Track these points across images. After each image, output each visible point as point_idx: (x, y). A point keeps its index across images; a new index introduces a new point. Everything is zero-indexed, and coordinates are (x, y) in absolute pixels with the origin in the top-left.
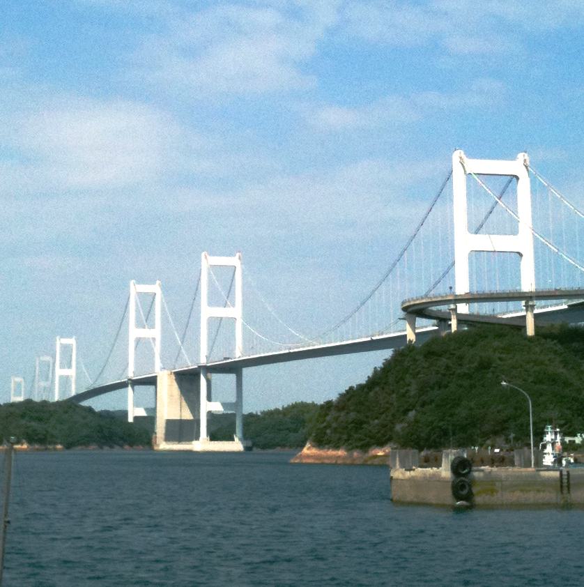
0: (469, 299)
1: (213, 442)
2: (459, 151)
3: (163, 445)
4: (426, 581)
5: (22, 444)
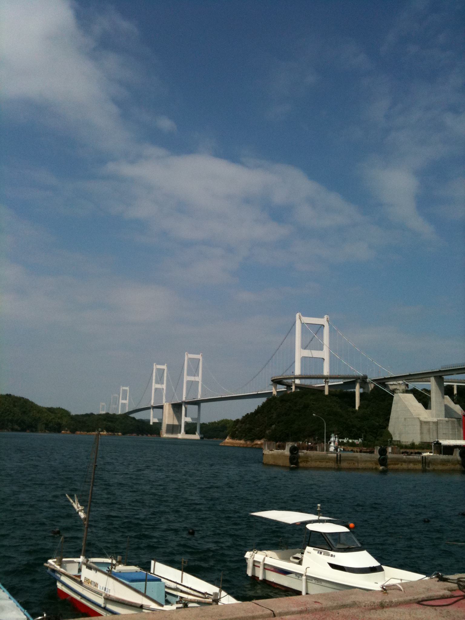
5: (104, 432)
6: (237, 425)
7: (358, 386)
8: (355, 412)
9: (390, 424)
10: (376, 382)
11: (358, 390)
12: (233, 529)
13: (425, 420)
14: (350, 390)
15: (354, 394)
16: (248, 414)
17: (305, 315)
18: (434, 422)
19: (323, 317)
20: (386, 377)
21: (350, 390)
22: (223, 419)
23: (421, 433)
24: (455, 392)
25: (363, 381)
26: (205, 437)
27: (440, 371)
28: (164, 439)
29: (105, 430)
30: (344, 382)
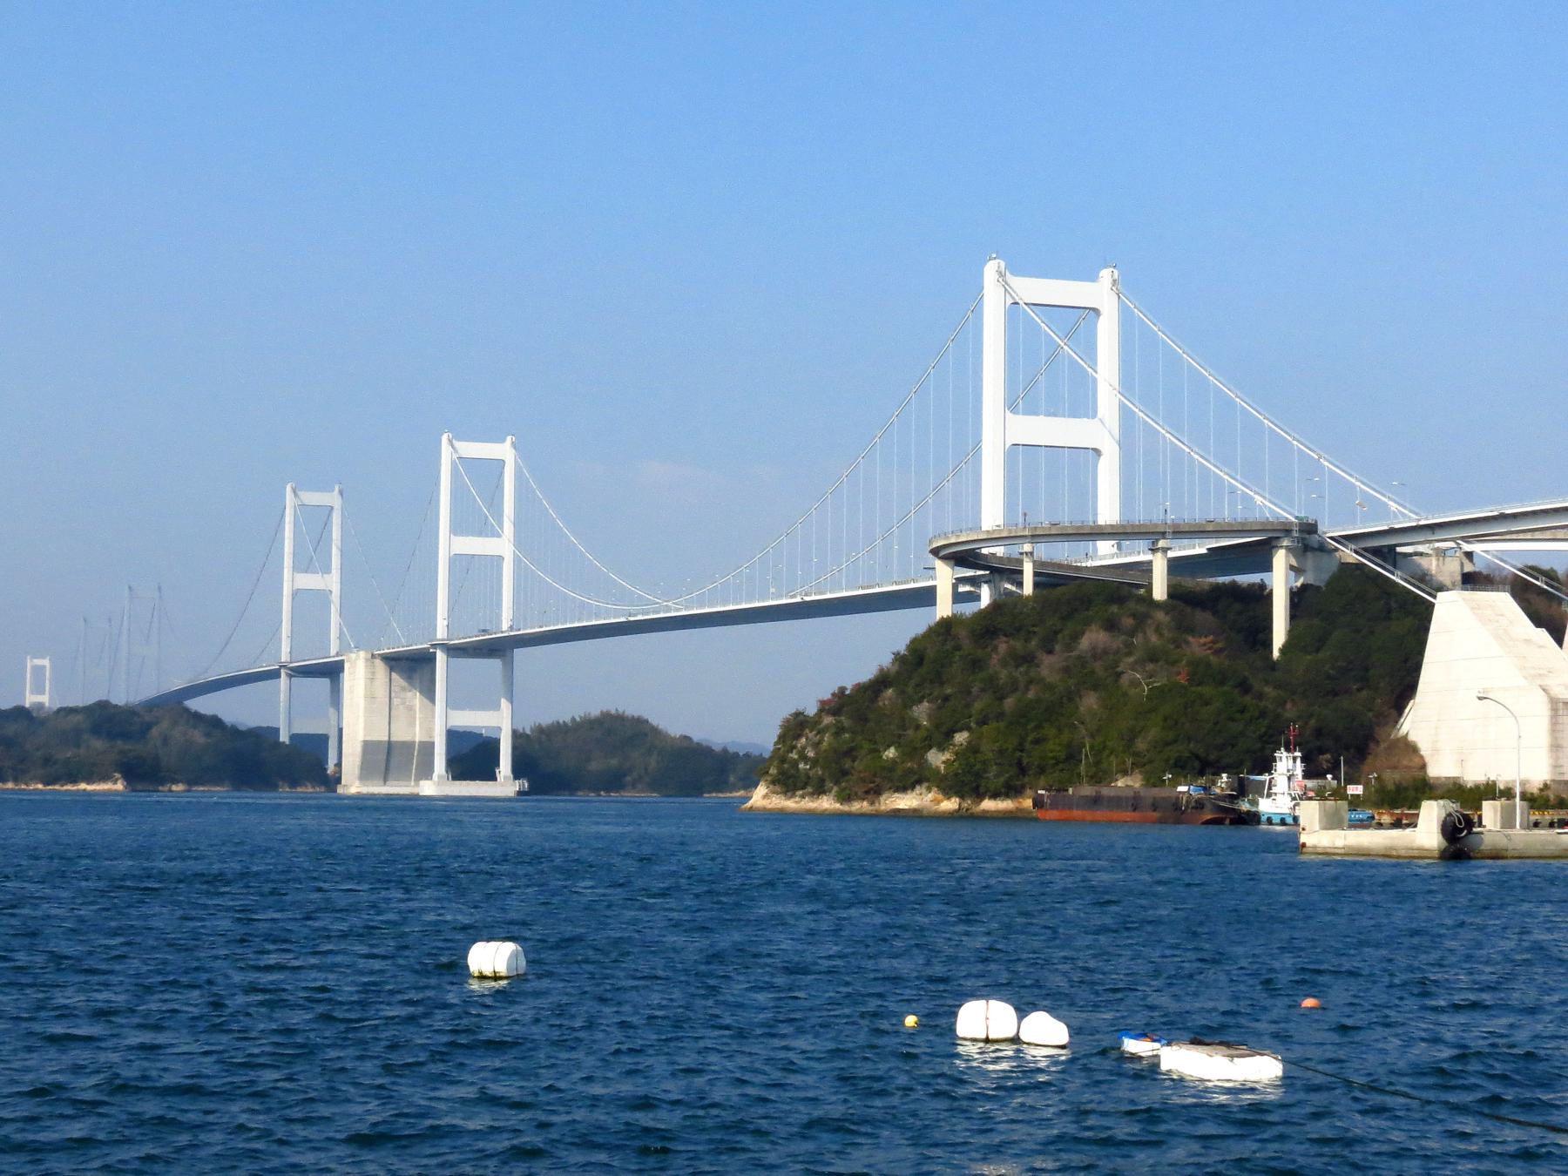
0: (1118, 533)
1: (458, 782)
2: (997, 261)
3: (353, 785)
4: (1252, 999)
5: (115, 783)
6: (798, 737)
7: (1280, 559)
8: (1273, 666)
10: (1353, 547)
11: (1280, 579)
14: (1212, 580)
15: (1262, 597)
16: (842, 690)
17: (1019, 266)
19: (1092, 277)
20: (1397, 526)
21: (1212, 580)
22: (573, 719)
25: (1307, 540)
26: (534, 790)
28: (383, 799)
29: (121, 772)
30: (1208, 549)
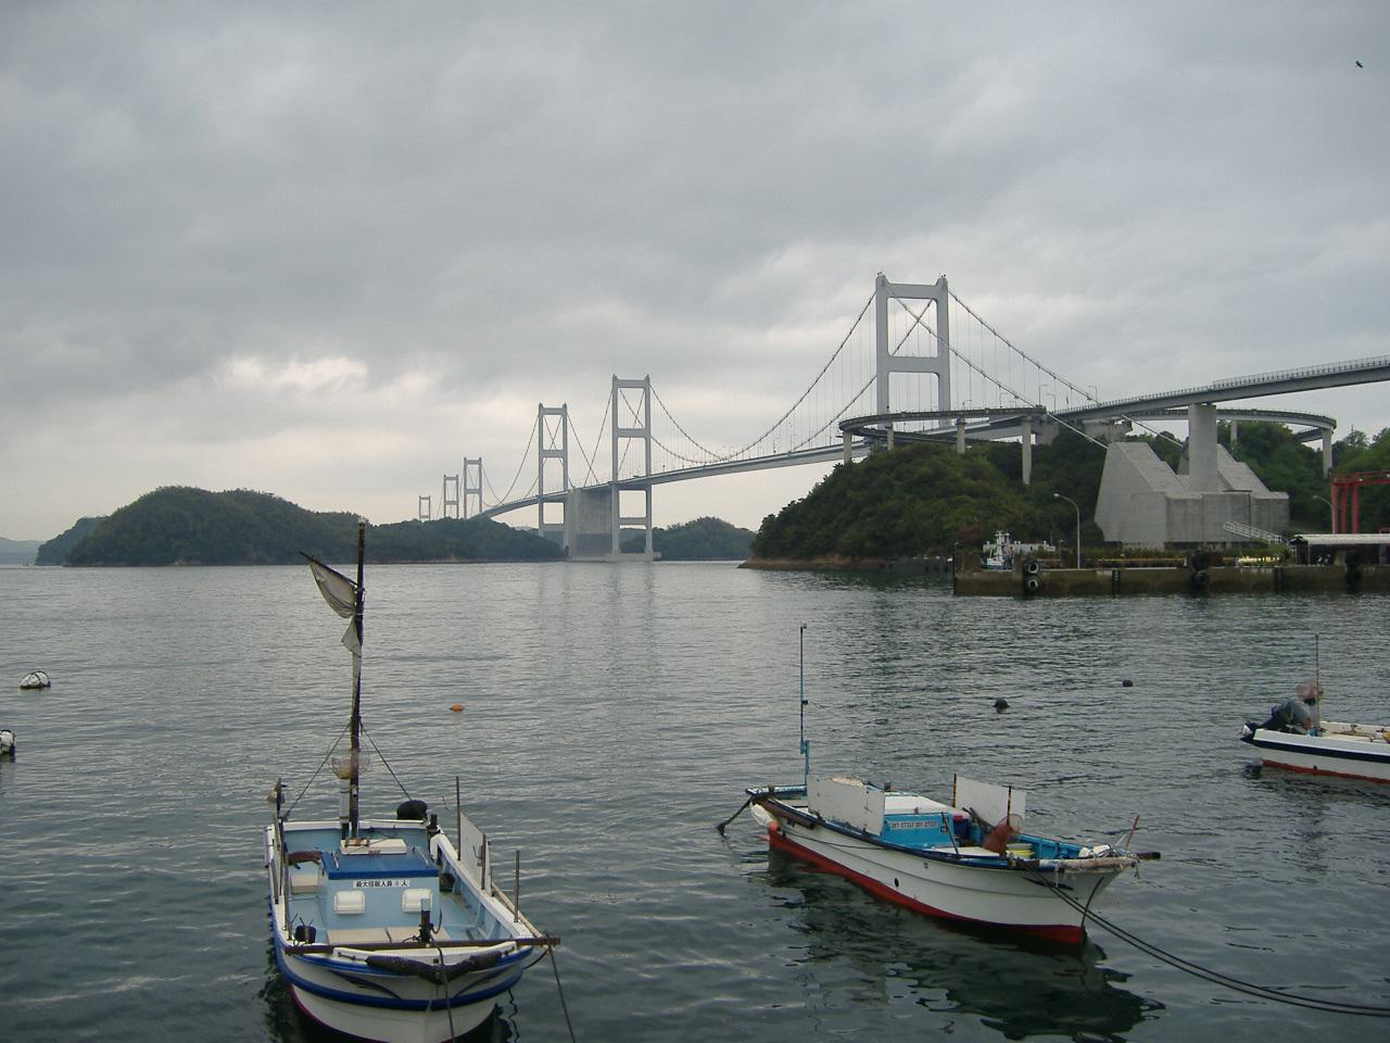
9: (1099, 508)
12: (939, 603)
13: (1178, 497)
18: (1195, 501)
23: (1169, 524)
24: (1234, 436)
27: (1210, 392)
